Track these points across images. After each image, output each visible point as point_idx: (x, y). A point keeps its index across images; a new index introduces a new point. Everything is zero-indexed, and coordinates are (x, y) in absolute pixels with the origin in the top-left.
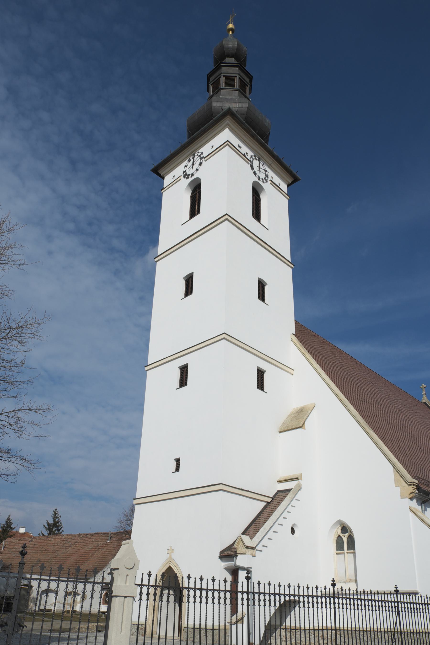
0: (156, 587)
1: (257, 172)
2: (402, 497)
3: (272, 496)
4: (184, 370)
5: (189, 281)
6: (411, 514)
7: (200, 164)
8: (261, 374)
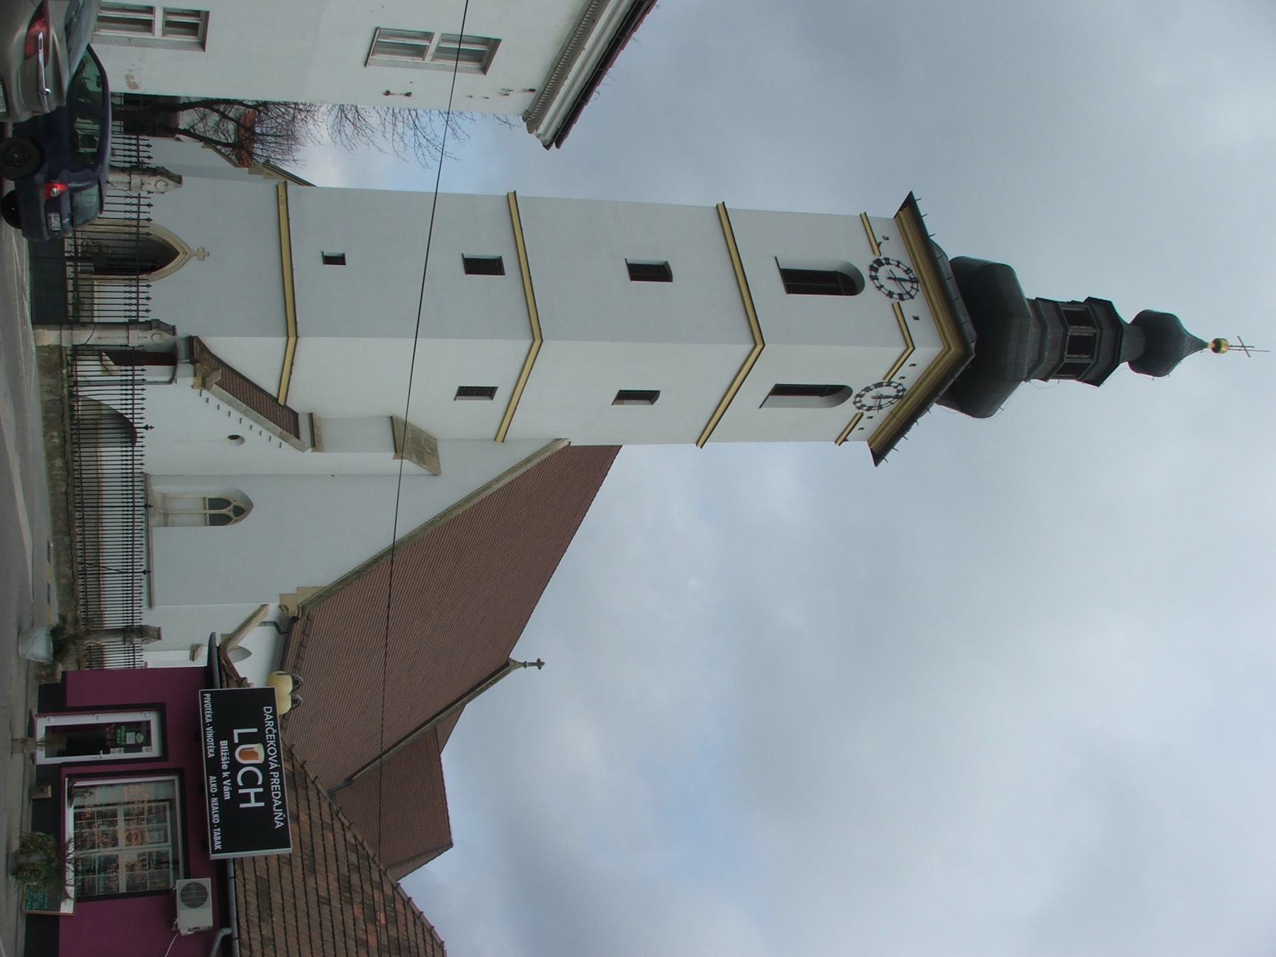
0: (138, 226)
1: (874, 392)
2: (282, 596)
3: (288, 404)
4: (490, 267)
5: (660, 273)
6: (258, 605)
7: (890, 294)
8: (489, 392)
